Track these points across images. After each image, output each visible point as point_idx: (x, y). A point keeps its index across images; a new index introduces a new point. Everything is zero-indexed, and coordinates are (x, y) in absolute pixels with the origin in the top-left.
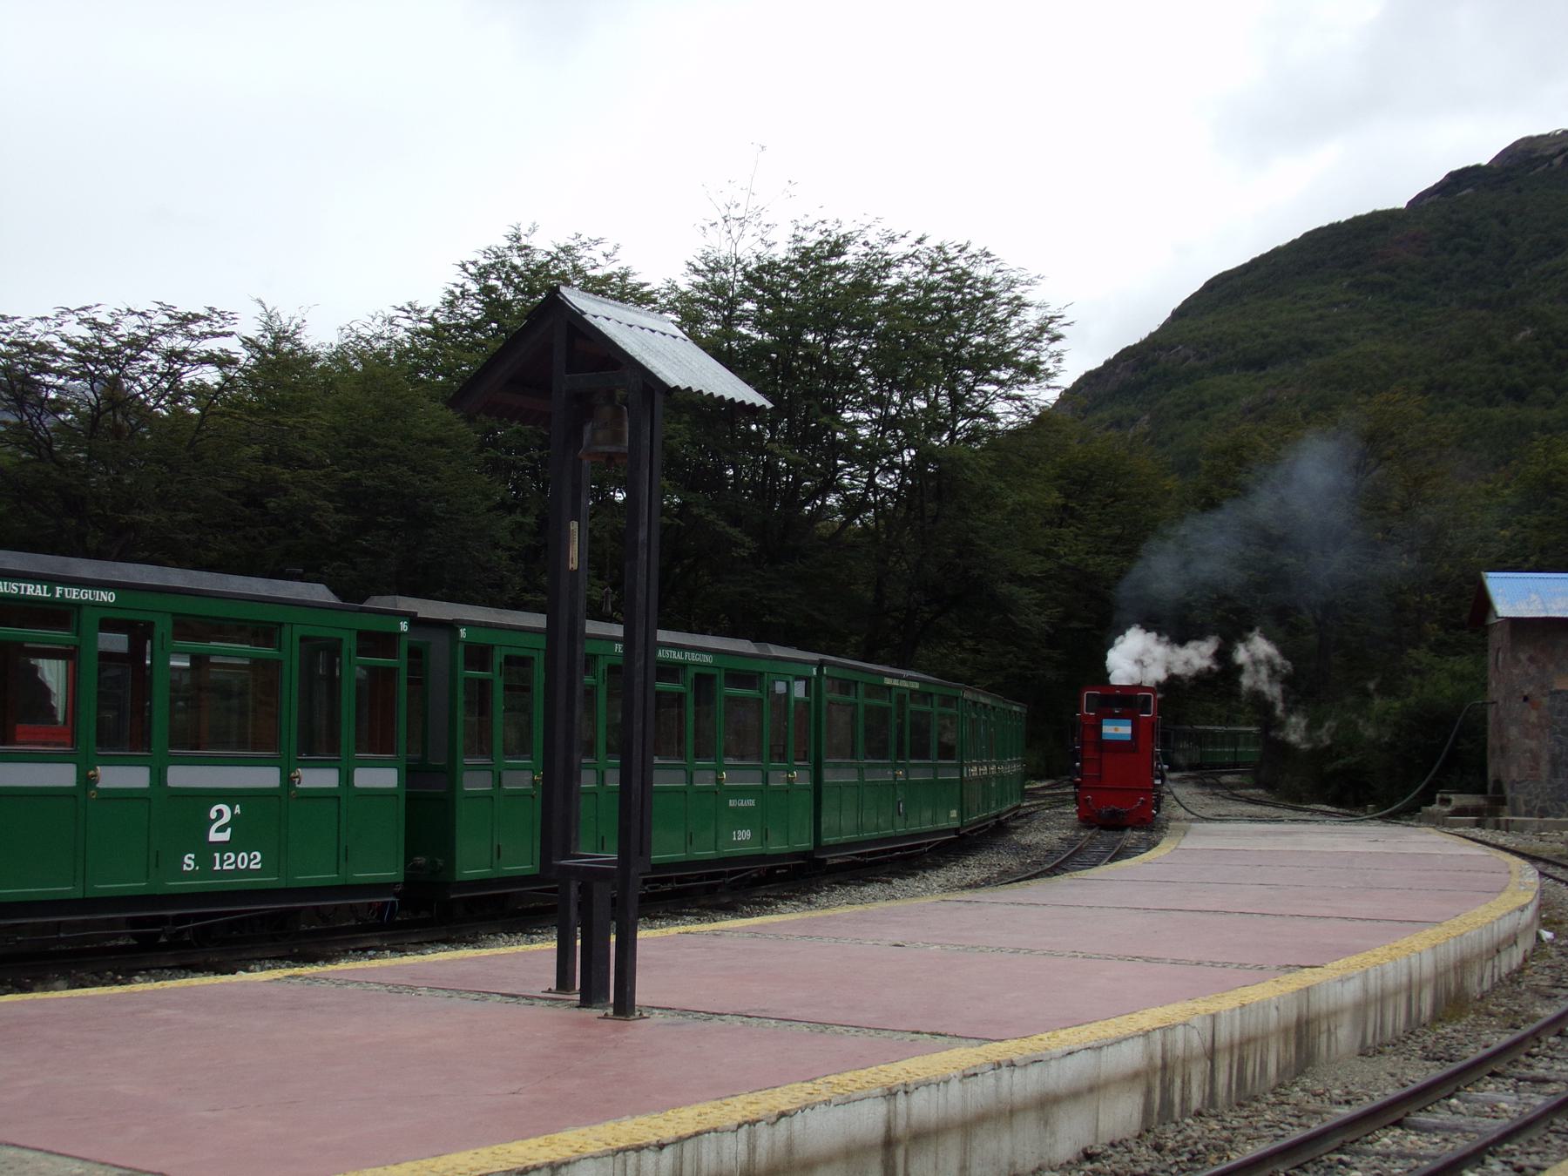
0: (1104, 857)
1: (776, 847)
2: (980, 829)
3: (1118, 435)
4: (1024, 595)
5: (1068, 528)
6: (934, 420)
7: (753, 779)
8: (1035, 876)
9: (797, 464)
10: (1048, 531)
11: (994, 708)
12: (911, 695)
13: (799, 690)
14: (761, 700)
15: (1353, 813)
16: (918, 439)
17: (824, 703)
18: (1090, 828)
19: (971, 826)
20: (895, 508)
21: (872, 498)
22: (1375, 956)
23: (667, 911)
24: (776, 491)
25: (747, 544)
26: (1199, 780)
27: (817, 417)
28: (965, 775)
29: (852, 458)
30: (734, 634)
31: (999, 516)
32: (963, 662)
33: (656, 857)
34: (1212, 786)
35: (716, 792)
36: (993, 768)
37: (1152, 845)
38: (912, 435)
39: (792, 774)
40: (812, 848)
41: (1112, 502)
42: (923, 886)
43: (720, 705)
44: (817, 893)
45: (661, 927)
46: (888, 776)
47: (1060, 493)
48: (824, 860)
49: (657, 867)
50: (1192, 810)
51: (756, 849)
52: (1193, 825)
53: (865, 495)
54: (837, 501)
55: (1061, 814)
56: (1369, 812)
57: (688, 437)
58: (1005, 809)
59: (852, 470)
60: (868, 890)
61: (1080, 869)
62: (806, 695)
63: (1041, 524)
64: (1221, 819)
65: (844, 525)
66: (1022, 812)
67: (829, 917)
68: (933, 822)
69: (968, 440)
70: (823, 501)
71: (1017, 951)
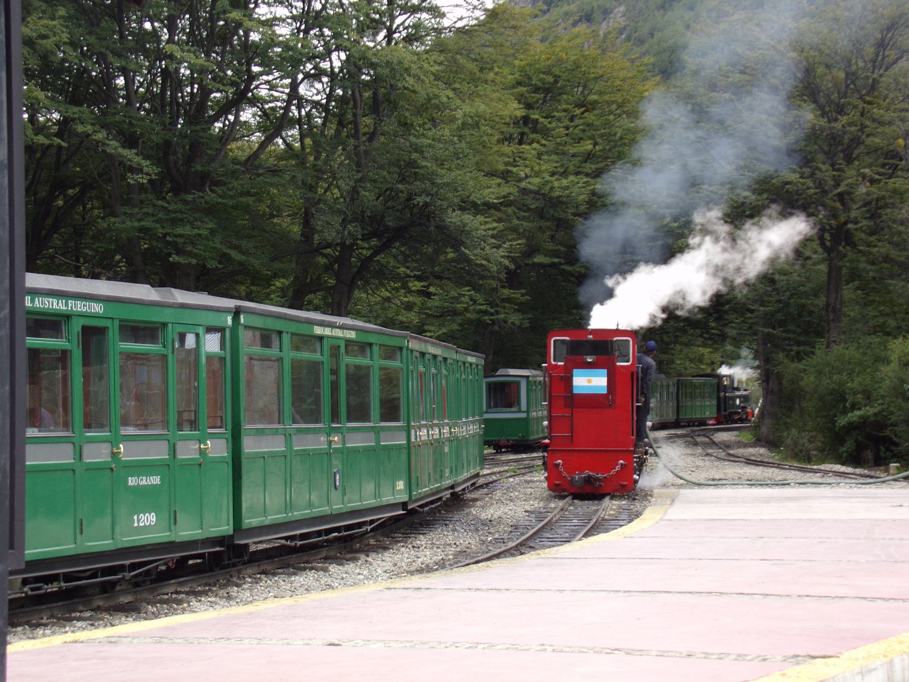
0: (578, 532)
1: (187, 531)
2: (432, 502)
3: (588, 31)
4: (477, 224)
5: (530, 144)
6: (367, 15)
7: (158, 452)
8: (498, 556)
9: (203, 71)
10: (506, 149)
11: (445, 359)
12: (346, 346)
13: (212, 344)
14: (164, 357)
15: (872, 473)
16: (349, 39)
17: (243, 359)
18: (563, 497)
19: (421, 499)
20: (324, 124)
21: (296, 113)
22: (901, 643)
23: (52, 616)
24: (178, 104)
25: (145, 170)
26: (689, 439)
27: (225, 12)
28: (413, 440)
29: (268, 65)
30: (133, 277)
31: (447, 132)
32: (409, 307)
33: (32, 552)
34: (705, 445)
35: (112, 469)
36: (446, 430)
37: (634, 516)
38: (341, 35)
39: (206, 444)
40: (231, 532)
41: (583, 113)
42: (365, 572)
43: (114, 363)
44: (238, 585)
45: (44, 635)
46: (319, 442)
47: (519, 103)
48: (246, 546)
49: (33, 565)
50: (681, 474)
51: (163, 536)
52: (682, 491)
53: (287, 109)
54: (254, 115)
55: (527, 482)
56: (891, 472)
57: (65, 37)
58: (461, 478)
59: (270, 78)
60: (300, 579)
61: (550, 547)
62: (221, 350)
63: (498, 141)
64: (716, 483)
65: (263, 145)
66: (481, 481)
67: (250, 614)
68: (377, 495)
69: (409, 39)
70: (237, 116)
71: (474, 646)
